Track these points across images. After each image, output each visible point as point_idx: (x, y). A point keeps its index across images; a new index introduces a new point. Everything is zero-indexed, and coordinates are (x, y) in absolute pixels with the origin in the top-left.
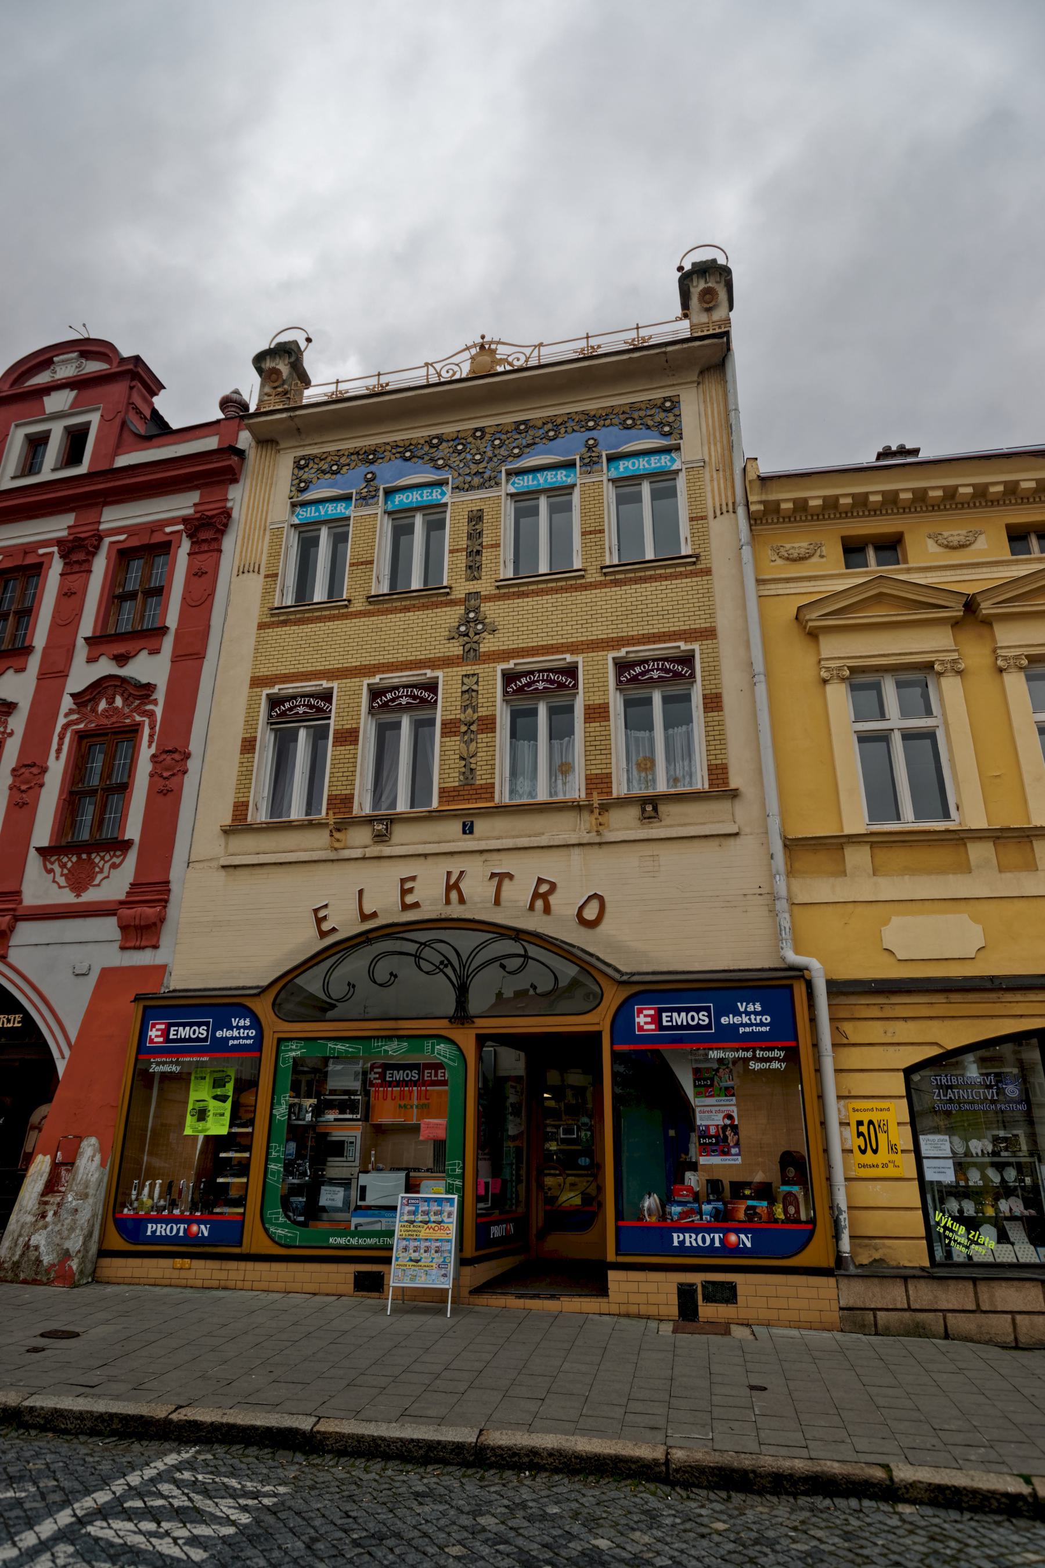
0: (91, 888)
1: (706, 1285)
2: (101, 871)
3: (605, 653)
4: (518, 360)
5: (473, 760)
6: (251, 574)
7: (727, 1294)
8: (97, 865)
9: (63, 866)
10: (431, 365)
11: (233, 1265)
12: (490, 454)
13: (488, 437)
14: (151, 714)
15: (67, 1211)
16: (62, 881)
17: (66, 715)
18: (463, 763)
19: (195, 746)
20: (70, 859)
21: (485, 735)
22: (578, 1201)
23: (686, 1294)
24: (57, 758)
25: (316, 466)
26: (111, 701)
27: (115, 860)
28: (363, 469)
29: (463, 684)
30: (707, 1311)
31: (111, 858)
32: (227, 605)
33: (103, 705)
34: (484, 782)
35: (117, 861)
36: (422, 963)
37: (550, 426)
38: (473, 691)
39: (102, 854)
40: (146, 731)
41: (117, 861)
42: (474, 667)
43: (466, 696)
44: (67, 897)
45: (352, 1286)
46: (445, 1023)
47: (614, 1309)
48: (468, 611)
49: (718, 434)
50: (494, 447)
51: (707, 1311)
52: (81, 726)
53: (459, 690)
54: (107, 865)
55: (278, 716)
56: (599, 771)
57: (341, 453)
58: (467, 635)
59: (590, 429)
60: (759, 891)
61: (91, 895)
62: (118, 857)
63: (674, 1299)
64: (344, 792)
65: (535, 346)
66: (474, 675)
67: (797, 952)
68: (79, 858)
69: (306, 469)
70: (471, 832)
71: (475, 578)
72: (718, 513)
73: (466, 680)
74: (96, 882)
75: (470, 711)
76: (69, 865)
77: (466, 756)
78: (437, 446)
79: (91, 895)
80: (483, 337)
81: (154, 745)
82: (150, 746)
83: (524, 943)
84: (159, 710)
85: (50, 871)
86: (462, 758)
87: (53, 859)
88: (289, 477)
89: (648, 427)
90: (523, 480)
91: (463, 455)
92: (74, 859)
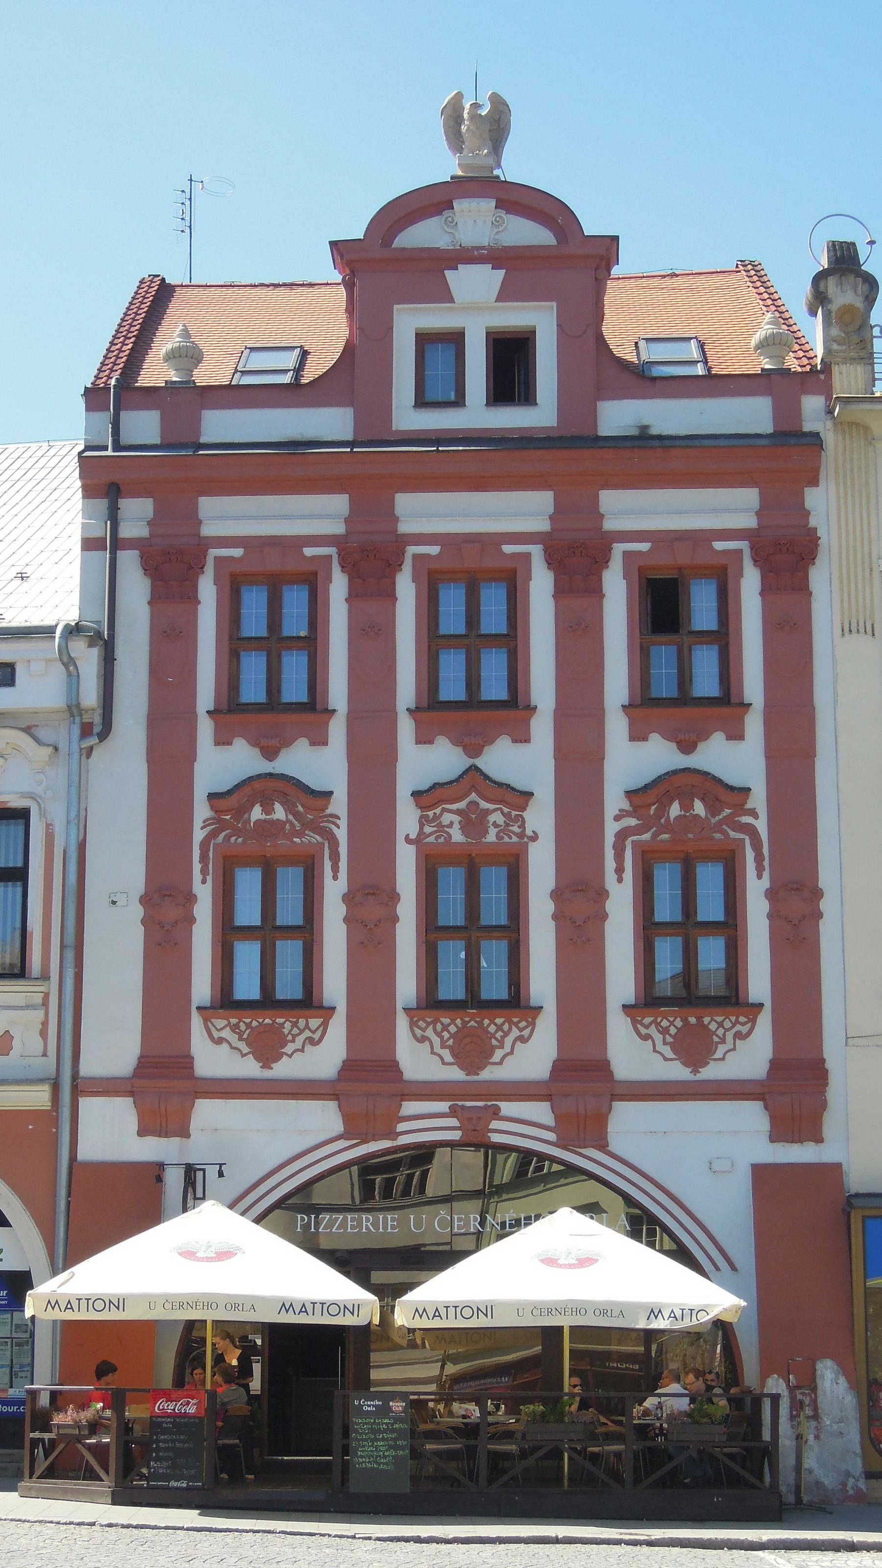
0: (712, 1063)
2: (723, 1041)
6: (855, 635)
8: (714, 1033)
9: (664, 1031)
14: (752, 832)
15: (107, 1427)
16: (668, 1052)
17: (617, 818)
19: (826, 878)
20: (672, 1023)
22: (683, 1404)
24: (335, 878)
26: (687, 806)
27: (738, 1027)
31: (734, 1025)
33: (675, 810)
35: (744, 1029)
39: (719, 1019)
40: (750, 855)
41: (744, 1029)
44: (678, 1072)
52: (647, 836)
54: (730, 1035)
61: (711, 1072)
62: (743, 1024)
68: (685, 1021)
72: (846, 629)
74: (719, 1054)
76: (673, 1031)
79: (711, 1072)
81: (766, 875)
82: (759, 876)
84: (762, 825)
85: (646, 1037)
87: (647, 1020)
92: (679, 1023)
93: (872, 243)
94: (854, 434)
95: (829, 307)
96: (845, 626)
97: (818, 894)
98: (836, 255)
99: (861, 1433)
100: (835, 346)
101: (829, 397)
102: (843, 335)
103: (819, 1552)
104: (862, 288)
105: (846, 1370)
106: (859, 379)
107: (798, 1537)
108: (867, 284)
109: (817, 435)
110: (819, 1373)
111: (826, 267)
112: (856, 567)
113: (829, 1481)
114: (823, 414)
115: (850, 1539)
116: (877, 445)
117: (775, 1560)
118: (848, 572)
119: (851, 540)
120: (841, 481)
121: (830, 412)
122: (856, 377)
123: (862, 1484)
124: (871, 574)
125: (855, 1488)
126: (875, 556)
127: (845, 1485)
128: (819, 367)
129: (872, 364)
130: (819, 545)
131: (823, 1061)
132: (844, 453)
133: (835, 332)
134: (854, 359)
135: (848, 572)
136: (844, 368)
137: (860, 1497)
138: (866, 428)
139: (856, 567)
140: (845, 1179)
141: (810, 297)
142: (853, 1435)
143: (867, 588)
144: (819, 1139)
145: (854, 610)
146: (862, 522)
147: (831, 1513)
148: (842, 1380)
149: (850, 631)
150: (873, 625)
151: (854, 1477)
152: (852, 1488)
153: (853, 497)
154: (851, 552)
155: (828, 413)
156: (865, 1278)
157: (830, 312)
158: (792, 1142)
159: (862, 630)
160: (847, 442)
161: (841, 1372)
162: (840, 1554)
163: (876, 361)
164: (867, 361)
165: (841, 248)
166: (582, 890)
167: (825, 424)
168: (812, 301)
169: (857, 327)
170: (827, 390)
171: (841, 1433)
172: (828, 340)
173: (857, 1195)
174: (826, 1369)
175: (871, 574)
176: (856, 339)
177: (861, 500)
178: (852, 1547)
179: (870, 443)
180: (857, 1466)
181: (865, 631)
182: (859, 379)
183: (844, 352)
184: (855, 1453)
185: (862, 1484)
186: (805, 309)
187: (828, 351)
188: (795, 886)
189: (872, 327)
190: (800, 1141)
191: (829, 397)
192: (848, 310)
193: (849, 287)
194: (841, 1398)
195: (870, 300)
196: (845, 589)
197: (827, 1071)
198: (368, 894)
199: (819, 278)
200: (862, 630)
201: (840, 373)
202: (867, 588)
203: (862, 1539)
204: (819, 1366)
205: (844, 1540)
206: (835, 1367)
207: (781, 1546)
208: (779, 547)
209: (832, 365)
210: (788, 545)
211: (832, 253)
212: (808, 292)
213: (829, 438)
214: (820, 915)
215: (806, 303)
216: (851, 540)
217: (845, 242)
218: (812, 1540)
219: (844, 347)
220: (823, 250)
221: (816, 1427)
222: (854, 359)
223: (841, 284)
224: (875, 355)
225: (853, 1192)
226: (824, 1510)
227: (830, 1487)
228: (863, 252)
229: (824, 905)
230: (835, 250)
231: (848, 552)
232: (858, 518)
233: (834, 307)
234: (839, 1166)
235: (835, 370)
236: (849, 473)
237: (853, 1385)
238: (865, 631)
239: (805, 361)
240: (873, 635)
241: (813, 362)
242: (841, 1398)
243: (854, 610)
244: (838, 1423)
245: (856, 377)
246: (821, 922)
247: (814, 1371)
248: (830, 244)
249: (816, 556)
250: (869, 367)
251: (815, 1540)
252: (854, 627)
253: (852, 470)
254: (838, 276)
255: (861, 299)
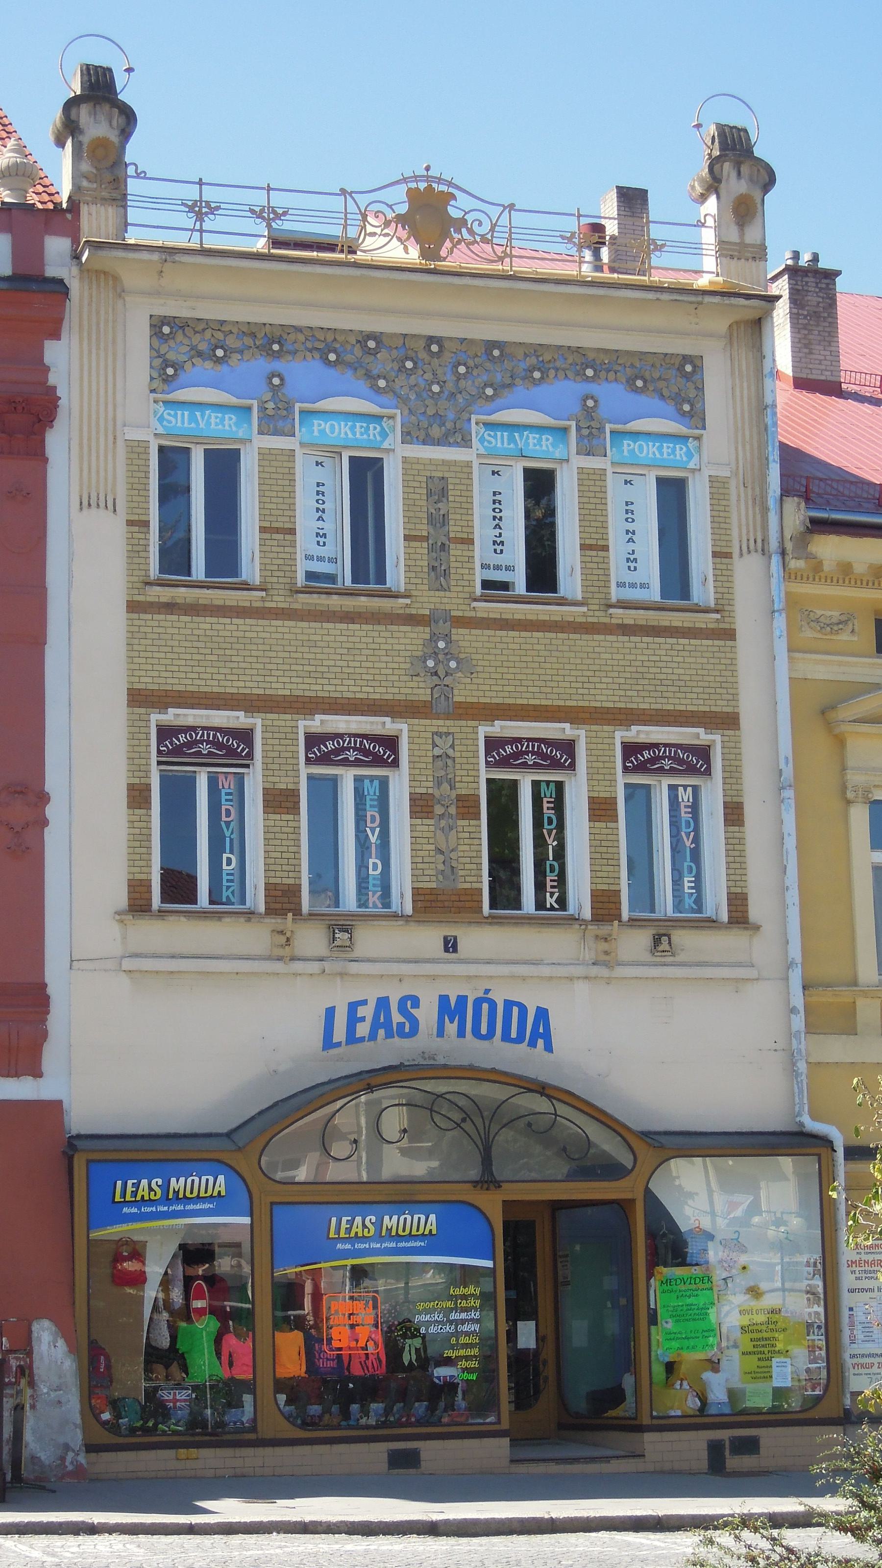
1: (734, 1441)
3: (611, 728)
4: (480, 224)
5: (453, 855)
6: (94, 510)
7: (750, 1446)
10: (350, 194)
11: (249, 1451)
12: (450, 386)
13: (447, 357)
18: (441, 858)
19: (54, 782)
21: (466, 822)
23: (715, 1449)
25: (186, 341)
28: (261, 365)
29: (435, 745)
30: (733, 1462)
32: (71, 560)
34: (467, 886)
36: (437, 1118)
37: (533, 360)
38: (448, 756)
42: (448, 723)
43: (440, 763)
45: (386, 1465)
46: (469, 1186)
47: (651, 1468)
48: (434, 638)
49: (747, 433)
50: (459, 377)
51: (733, 1462)
53: (430, 754)
55: (170, 753)
56: (605, 887)
57: (226, 328)
58: (436, 674)
59: (587, 379)
60: (774, 1046)
63: (705, 1455)
64: (285, 881)
65: (505, 208)
66: (448, 734)
67: (814, 1117)
69: (171, 343)
70: (455, 950)
71: (442, 588)
72: (85, 503)
73: (437, 740)
75: (446, 786)
77: (444, 849)
78: (374, 353)
80: (428, 169)
83: (554, 1101)
86: (440, 851)
88: (147, 352)
89: (662, 397)
90: (495, 437)
91: (413, 380)
93: (129, 70)
94: (102, 284)
95: (81, 138)
96: (92, 497)
97: (43, 798)
98: (90, 80)
99: (81, 1401)
100: (85, 183)
101: (76, 241)
102: (94, 171)
103: (56, 1536)
104: (118, 120)
105: (66, 1331)
106: (110, 223)
107: (33, 1520)
108: (124, 117)
109: (61, 282)
110: (35, 1335)
111: (78, 93)
112: (98, 433)
113: (46, 1456)
114: (68, 259)
115: (90, 1521)
116: (127, 299)
117: (15, 1546)
118: (89, 439)
119: (94, 403)
120: (85, 334)
121: (77, 257)
122: (107, 219)
123: (82, 1459)
124: (114, 443)
125: (75, 1463)
126: (119, 423)
127: (63, 1459)
128: (64, 206)
129: (125, 207)
130: (58, 406)
131: (44, 986)
132: (90, 304)
133: (86, 167)
134: (105, 199)
135: (89, 439)
136: (93, 208)
137: (79, 1472)
138: (116, 279)
139: (98, 433)
140: (66, 1118)
141: (59, 124)
142: (73, 1403)
143: (110, 457)
144: (37, 1074)
145: (94, 481)
146: (106, 381)
147: (54, 1492)
148: (61, 1343)
149: (89, 505)
150: (114, 499)
151: (73, 1451)
152: (72, 1463)
153: (98, 354)
154: (94, 417)
155: (74, 258)
156: (88, 1229)
157: (81, 143)
158: (8, 1076)
159: (102, 504)
160: (94, 293)
161: (60, 1335)
162: (80, 1537)
163: (129, 203)
164: (120, 203)
165: (96, 73)
166: (22, 792)
167: (70, 270)
168: (61, 130)
169: (110, 163)
170: (74, 234)
171: (59, 1402)
172: (77, 175)
173: (79, 1137)
174: (43, 1331)
175: (114, 443)
176: (108, 177)
177: (106, 360)
178: (92, 1530)
179: (120, 296)
180: (76, 1438)
181: (98, 505)
182: (110, 223)
183: (95, 190)
184: (75, 1424)
185: (82, 1459)
186: (51, 138)
187: (77, 188)
188: (19, 789)
189: (126, 165)
190: (17, 1075)
191: (76, 241)
192: (101, 144)
193: (103, 118)
194: (59, 1363)
195: (126, 133)
196: (86, 458)
197: (47, 998)
198: (16, 792)
199: (71, 105)
200: (102, 504)
201: (90, 214)
202: (110, 457)
203: (103, 1521)
204: (35, 1327)
205: (83, 1522)
206: (54, 1328)
207: (14, 1530)
208: (13, 405)
209: (81, 204)
210: (24, 404)
211: (86, 78)
212: (58, 119)
213: (75, 286)
214: (45, 822)
215: (53, 132)
216: (94, 403)
217: (100, 67)
218: (48, 1523)
219: (95, 185)
220: (75, 74)
221: (32, 1396)
222: (105, 199)
223: (95, 114)
224: (129, 197)
225: (74, 1132)
226: (43, 1488)
227: (47, 1462)
228: (120, 80)
229: (51, 811)
230: (89, 74)
231: (90, 416)
232: (102, 379)
233: (86, 139)
234: (60, 1103)
235: (84, 209)
236: (94, 328)
237: (73, 1348)
238: (98, 505)
239: (46, 198)
240: (115, 510)
241: (56, 199)
242: (59, 1363)
243: (94, 481)
244: (56, 1390)
245: (107, 219)
246: (46, 830)
247: (30, 1332)
248: (84, 68)
249: (55, 418)
250: (121, 210)
251: (52, 1522)
252: (93, 502)
253: (98, 324)
254: (92, 104)
255: (117, 132)
